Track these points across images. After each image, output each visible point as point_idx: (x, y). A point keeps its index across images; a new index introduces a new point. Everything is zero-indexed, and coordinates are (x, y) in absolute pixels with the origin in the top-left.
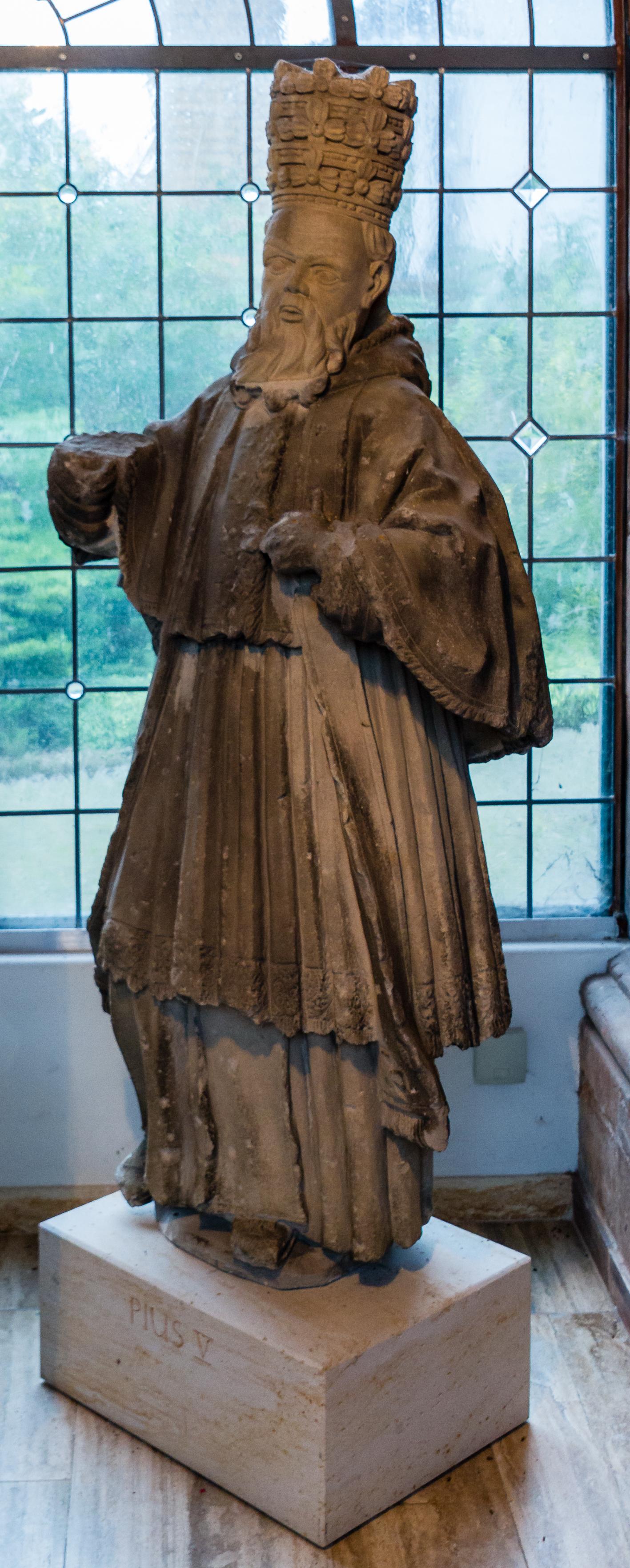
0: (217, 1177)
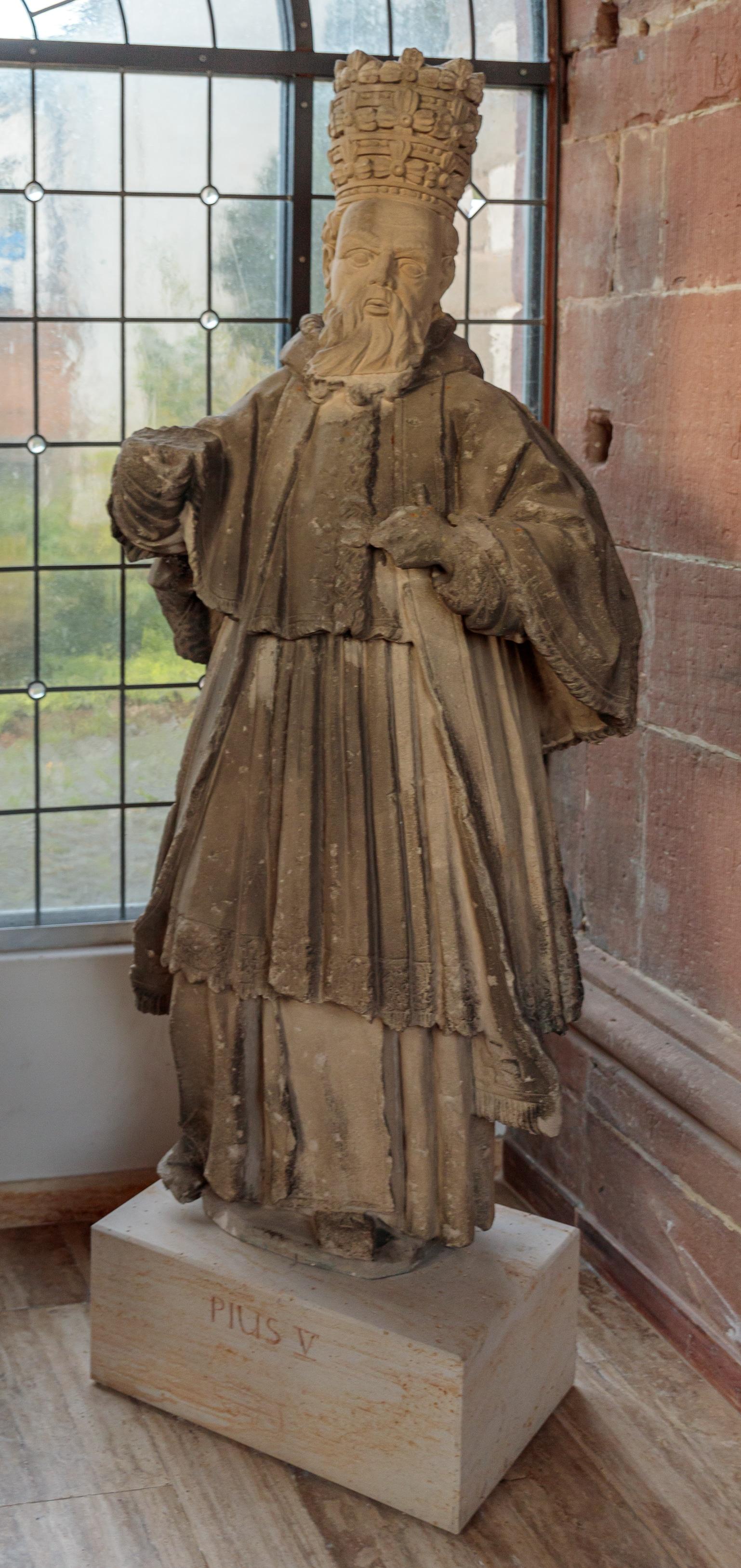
0: (296, 1172)
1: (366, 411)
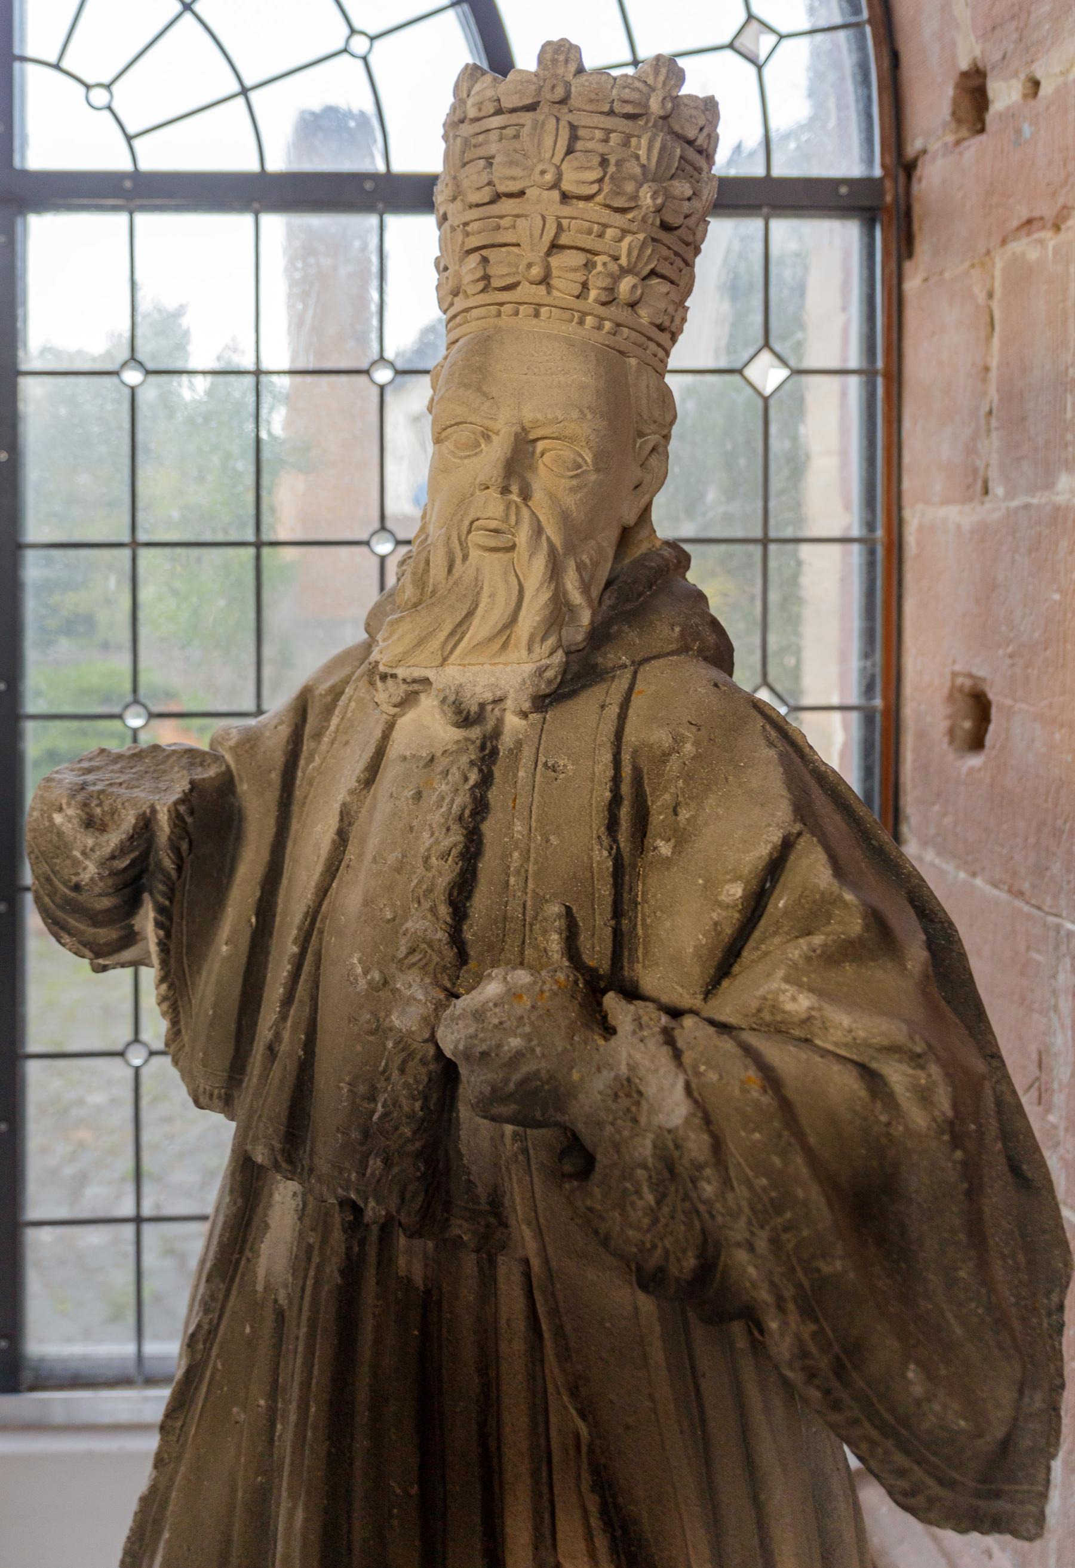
1: (467, 739)
